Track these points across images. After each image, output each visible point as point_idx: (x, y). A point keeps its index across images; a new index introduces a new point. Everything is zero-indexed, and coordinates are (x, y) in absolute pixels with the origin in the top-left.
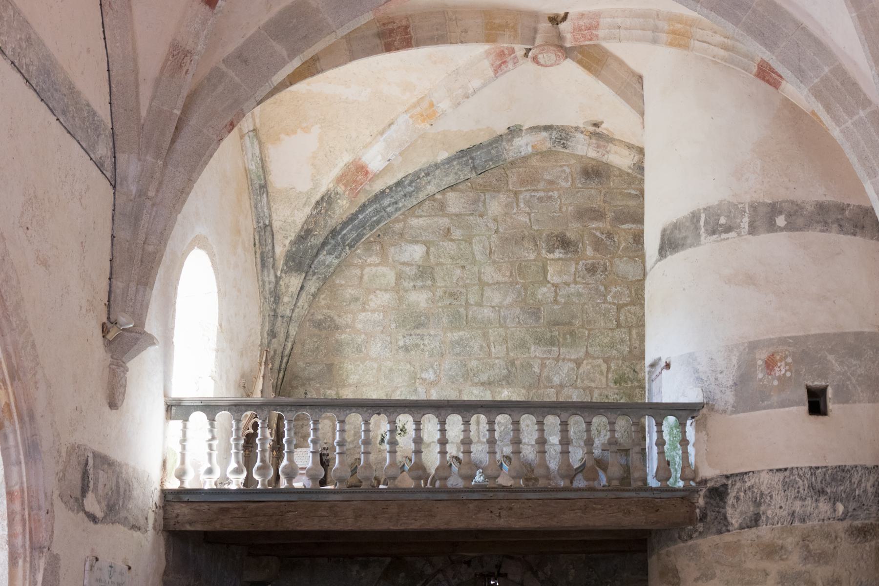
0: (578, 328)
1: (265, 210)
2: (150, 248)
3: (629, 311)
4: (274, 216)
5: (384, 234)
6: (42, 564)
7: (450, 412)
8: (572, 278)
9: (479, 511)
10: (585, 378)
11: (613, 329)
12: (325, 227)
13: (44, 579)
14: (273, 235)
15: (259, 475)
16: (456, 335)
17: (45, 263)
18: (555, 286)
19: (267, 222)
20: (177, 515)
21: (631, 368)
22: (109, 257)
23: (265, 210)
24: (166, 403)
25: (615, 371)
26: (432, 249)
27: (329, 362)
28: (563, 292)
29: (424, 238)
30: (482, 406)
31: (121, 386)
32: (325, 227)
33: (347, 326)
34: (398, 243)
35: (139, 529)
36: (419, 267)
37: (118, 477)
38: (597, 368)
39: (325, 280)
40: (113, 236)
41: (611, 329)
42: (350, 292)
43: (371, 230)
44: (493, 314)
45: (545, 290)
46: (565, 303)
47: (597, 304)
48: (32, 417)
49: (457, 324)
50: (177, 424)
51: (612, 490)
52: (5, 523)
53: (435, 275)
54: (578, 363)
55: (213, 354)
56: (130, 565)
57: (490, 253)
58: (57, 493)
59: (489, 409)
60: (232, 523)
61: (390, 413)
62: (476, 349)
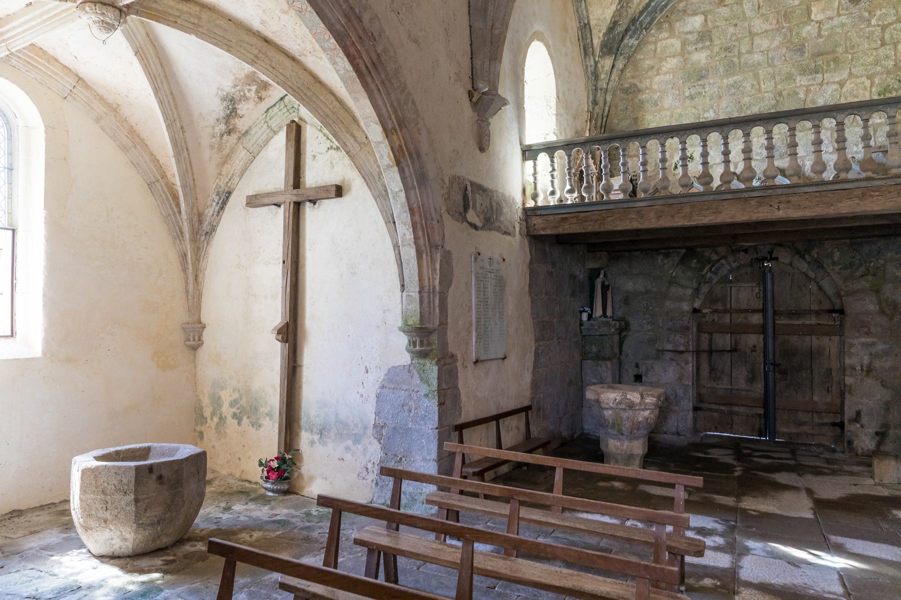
0: (842, 54)
1: (584, 13)
2: (496, 32)
3: (895, 29)
4: (591, 17)
5: (671, 14)
6: (438, 257)
7: (732, 128)
8: (836, 12)
9: (760, 206)
10: (848, 95)
11: (877, 48)
12: (627, 16)
13: (440, 267)
14: (591, 31)
15: (586, 193)
16: (731, 80)
17: (416, 41)
18: (819, 22)
19: (586, 22)
20: (535, 225)
21: (896, 79)
22: (469, 43)
23: (584, 13)
24: (522, 149)
25: (879, 84)
26: (709, 17)
27: (635, 117)
28: (826, 26)
29: (702, 10)
30: (760, 120)
31: (486, 135)
32: (627, 16)
33: (647, 88)
34: (682, 18)
35: (509, 234)
36: (700, 33)
37: (491, 200)
38: (860, 85)
39: (629, 58)
40: (470, 27)
41: (875, 49)
42: (648, 63)
43: (661, 13)
44: (762, 58)
45: (809, 28)
46: (828, 35)
47: (861, 30)
48: (419, 155)
49: (732, 71)
50: (529, 164)
51: (892, 177)
52: (411, 230)
53: (713, 36)
54: (841, 84)
55: (554, 118)
56: (505, 258)
57: (759, 8)
58: (444, 209)
59: (767, 121)
60: (570, 228)
61: (681, 136)
62: (748, 88)
